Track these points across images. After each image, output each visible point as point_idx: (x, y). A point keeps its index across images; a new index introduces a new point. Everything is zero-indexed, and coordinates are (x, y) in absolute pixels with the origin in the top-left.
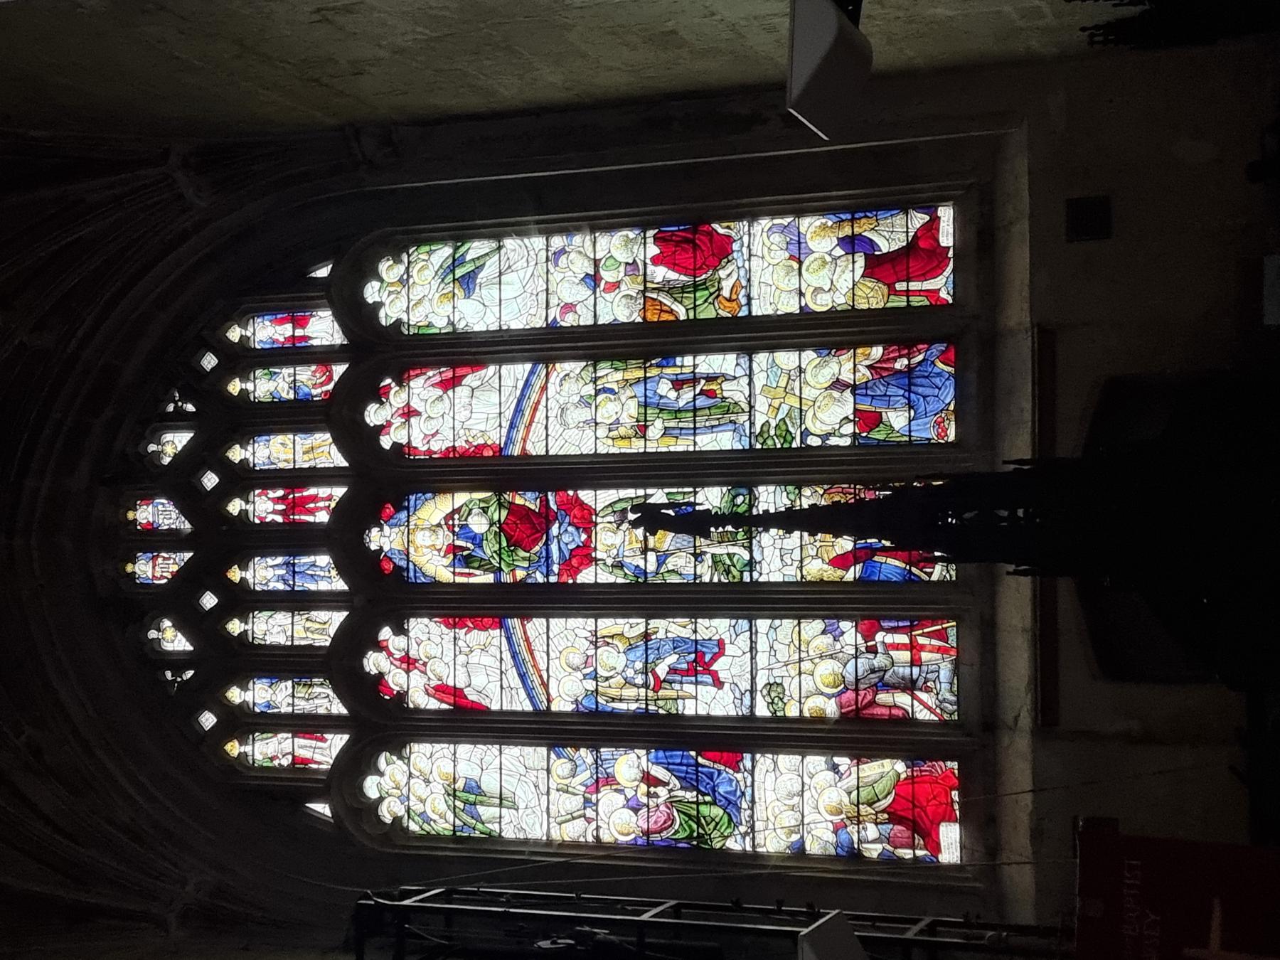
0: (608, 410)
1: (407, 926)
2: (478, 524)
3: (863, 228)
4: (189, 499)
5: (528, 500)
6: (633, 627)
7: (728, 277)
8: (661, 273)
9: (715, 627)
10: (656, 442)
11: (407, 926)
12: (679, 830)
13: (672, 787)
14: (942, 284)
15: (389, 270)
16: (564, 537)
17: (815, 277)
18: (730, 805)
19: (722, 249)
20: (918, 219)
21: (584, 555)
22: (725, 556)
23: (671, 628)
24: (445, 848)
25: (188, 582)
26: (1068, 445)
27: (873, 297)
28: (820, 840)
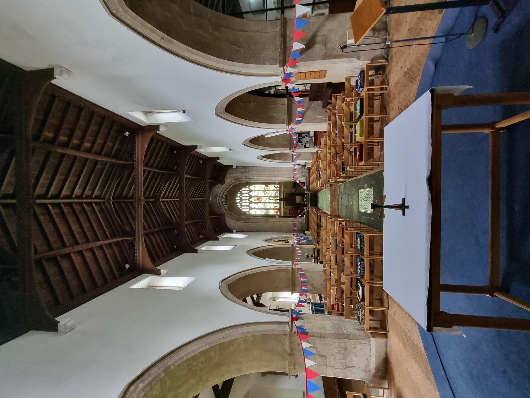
0: (262, 194)
1: (465, 336)
2: (256, 199)
3: (275, 186)
4: (240, 197)
5: (258, 198)
6: (264, 204)
7: (269, 188)
8: (265, 187)
9: (268, 204)
10: (265, 195)
11: (465, 336)
12: (266, 213)
13: (266, 211)
14: (279, 189)
15: (251, 186)
16: (260, 200)
17: (273, 188)
18: (269, 212)
19: (268, 186)
20: (278, 186)
21: (261, 201)
22: (80, 242)
23: (266, 204)
24: (152, 181)
25: (240, 202)
26: (284, 197)
27: (275, 189)
28: (273, 214)
